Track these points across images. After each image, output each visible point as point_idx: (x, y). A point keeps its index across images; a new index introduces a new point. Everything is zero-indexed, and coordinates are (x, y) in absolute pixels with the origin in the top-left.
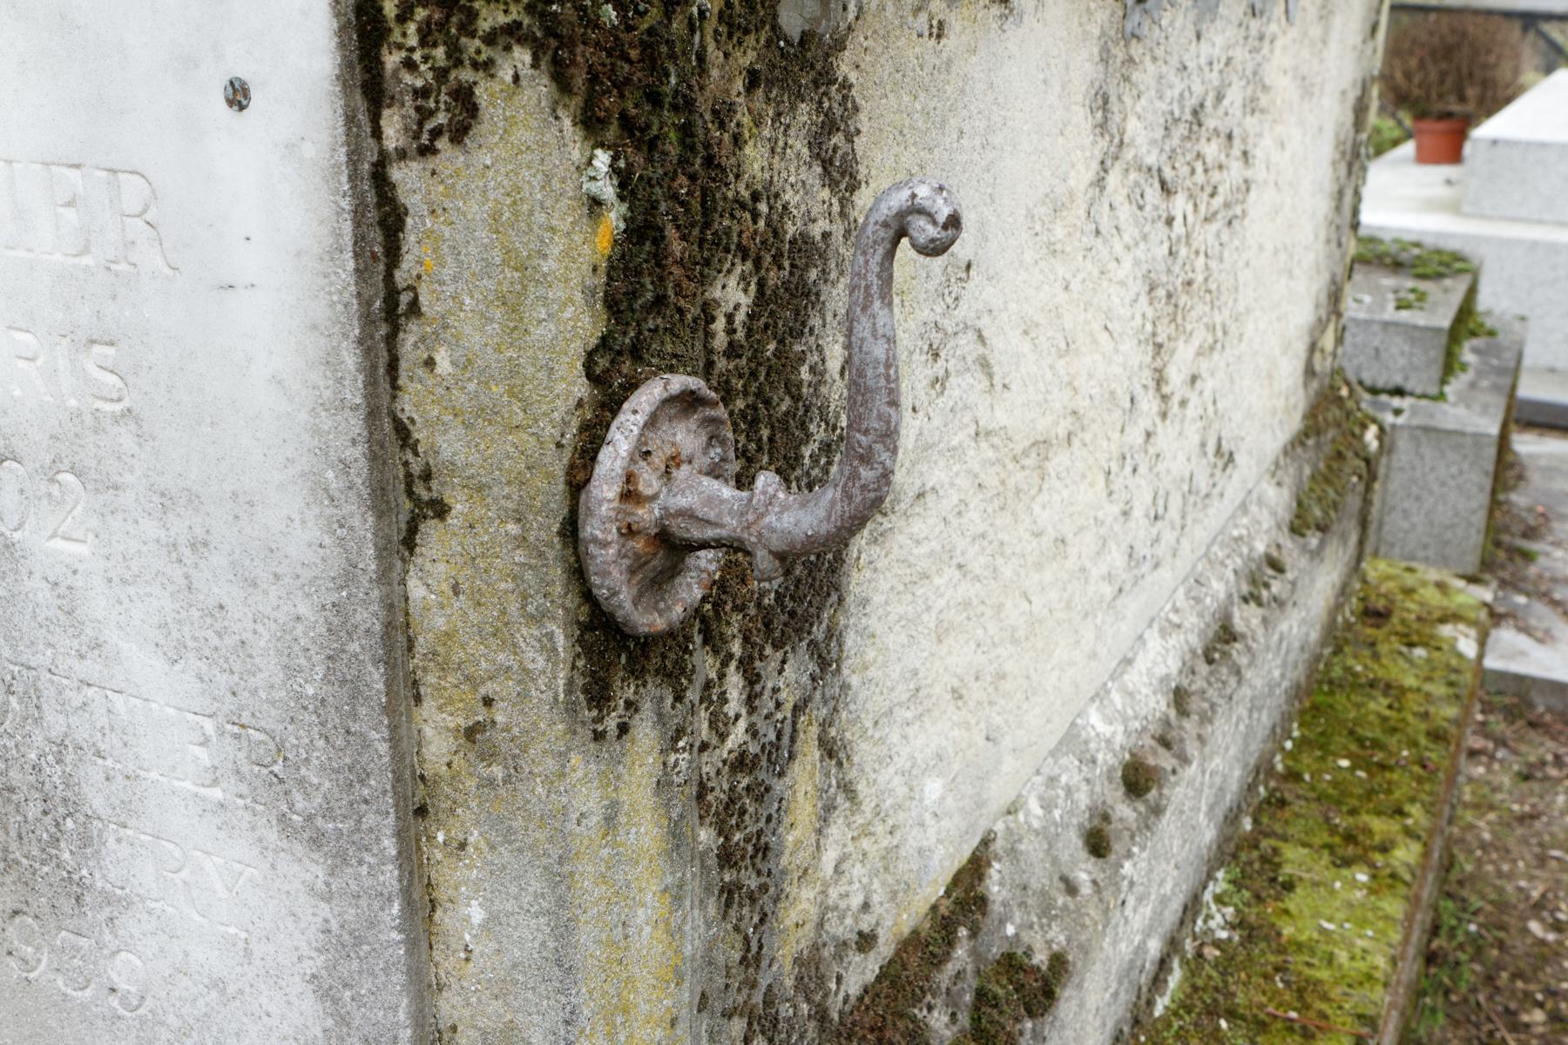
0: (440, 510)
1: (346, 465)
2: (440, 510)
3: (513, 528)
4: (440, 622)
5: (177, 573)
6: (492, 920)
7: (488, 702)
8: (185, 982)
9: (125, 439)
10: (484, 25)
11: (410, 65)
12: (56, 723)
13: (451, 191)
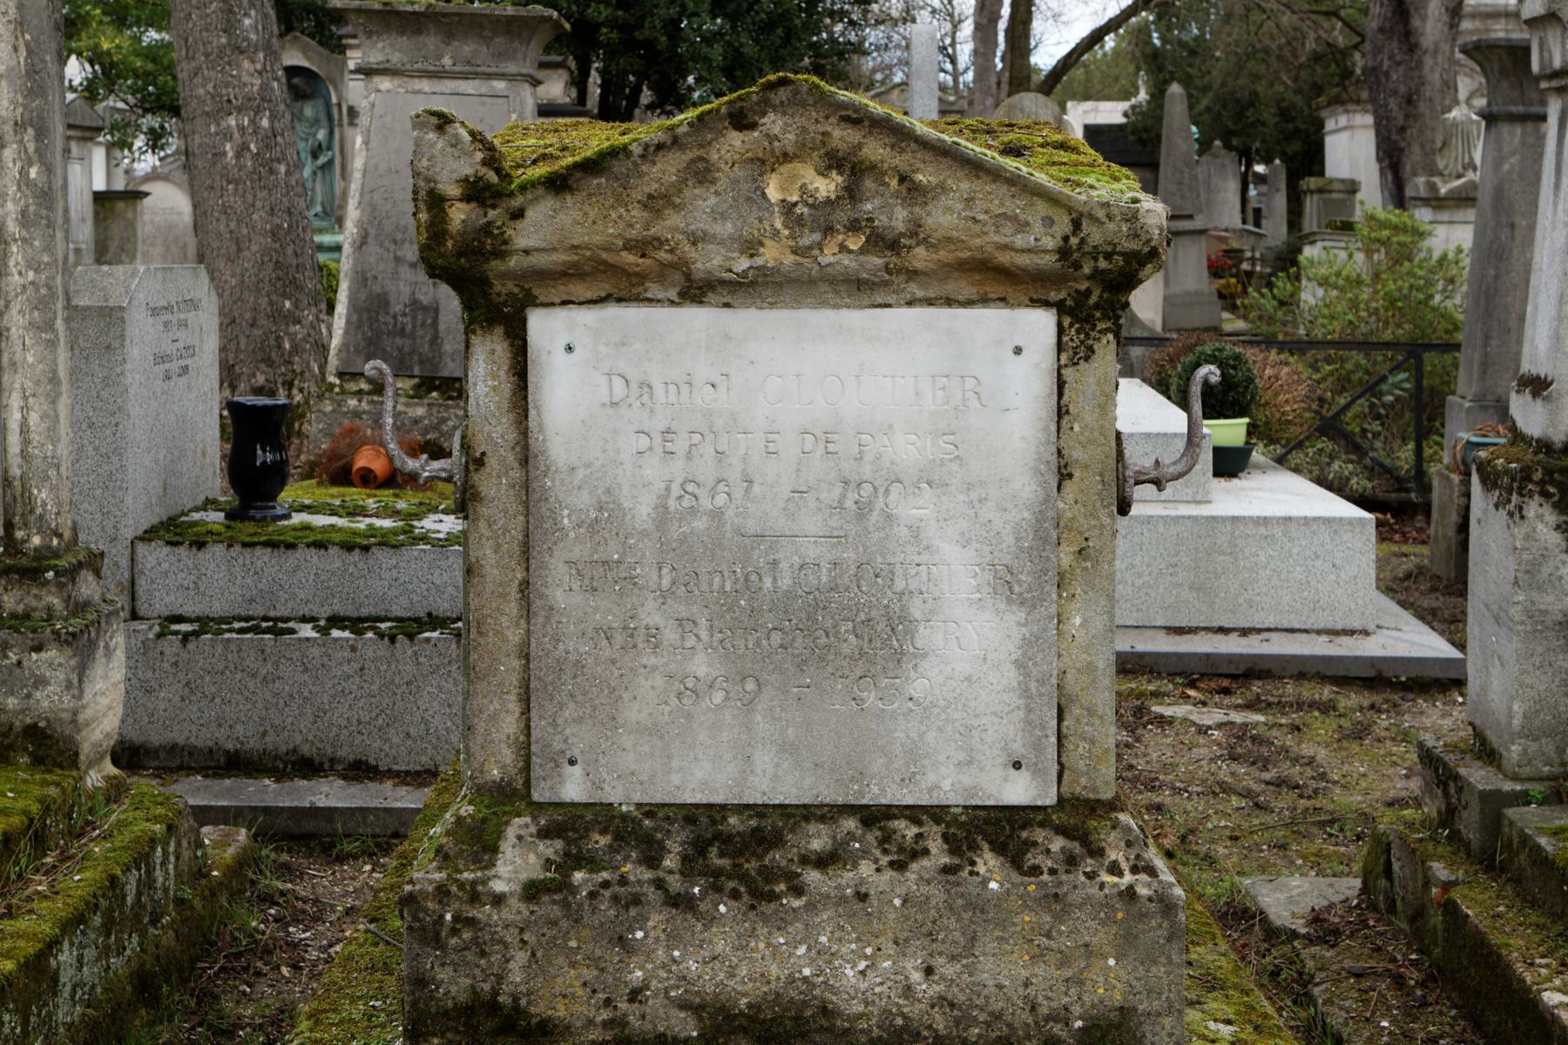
0: (1070, 476)
1: (1048, 462)
2: (1070, 476)
3: (1098, 478)
4: (1069, 515)
5: (972, 513)
6: (1085, 621)
7: (1086, 539)
8: (951, 682)
9: (955, 467)
10: (1098, 328)
11: (1072, 340)
12: (900, 584)
13: (1083, 376)
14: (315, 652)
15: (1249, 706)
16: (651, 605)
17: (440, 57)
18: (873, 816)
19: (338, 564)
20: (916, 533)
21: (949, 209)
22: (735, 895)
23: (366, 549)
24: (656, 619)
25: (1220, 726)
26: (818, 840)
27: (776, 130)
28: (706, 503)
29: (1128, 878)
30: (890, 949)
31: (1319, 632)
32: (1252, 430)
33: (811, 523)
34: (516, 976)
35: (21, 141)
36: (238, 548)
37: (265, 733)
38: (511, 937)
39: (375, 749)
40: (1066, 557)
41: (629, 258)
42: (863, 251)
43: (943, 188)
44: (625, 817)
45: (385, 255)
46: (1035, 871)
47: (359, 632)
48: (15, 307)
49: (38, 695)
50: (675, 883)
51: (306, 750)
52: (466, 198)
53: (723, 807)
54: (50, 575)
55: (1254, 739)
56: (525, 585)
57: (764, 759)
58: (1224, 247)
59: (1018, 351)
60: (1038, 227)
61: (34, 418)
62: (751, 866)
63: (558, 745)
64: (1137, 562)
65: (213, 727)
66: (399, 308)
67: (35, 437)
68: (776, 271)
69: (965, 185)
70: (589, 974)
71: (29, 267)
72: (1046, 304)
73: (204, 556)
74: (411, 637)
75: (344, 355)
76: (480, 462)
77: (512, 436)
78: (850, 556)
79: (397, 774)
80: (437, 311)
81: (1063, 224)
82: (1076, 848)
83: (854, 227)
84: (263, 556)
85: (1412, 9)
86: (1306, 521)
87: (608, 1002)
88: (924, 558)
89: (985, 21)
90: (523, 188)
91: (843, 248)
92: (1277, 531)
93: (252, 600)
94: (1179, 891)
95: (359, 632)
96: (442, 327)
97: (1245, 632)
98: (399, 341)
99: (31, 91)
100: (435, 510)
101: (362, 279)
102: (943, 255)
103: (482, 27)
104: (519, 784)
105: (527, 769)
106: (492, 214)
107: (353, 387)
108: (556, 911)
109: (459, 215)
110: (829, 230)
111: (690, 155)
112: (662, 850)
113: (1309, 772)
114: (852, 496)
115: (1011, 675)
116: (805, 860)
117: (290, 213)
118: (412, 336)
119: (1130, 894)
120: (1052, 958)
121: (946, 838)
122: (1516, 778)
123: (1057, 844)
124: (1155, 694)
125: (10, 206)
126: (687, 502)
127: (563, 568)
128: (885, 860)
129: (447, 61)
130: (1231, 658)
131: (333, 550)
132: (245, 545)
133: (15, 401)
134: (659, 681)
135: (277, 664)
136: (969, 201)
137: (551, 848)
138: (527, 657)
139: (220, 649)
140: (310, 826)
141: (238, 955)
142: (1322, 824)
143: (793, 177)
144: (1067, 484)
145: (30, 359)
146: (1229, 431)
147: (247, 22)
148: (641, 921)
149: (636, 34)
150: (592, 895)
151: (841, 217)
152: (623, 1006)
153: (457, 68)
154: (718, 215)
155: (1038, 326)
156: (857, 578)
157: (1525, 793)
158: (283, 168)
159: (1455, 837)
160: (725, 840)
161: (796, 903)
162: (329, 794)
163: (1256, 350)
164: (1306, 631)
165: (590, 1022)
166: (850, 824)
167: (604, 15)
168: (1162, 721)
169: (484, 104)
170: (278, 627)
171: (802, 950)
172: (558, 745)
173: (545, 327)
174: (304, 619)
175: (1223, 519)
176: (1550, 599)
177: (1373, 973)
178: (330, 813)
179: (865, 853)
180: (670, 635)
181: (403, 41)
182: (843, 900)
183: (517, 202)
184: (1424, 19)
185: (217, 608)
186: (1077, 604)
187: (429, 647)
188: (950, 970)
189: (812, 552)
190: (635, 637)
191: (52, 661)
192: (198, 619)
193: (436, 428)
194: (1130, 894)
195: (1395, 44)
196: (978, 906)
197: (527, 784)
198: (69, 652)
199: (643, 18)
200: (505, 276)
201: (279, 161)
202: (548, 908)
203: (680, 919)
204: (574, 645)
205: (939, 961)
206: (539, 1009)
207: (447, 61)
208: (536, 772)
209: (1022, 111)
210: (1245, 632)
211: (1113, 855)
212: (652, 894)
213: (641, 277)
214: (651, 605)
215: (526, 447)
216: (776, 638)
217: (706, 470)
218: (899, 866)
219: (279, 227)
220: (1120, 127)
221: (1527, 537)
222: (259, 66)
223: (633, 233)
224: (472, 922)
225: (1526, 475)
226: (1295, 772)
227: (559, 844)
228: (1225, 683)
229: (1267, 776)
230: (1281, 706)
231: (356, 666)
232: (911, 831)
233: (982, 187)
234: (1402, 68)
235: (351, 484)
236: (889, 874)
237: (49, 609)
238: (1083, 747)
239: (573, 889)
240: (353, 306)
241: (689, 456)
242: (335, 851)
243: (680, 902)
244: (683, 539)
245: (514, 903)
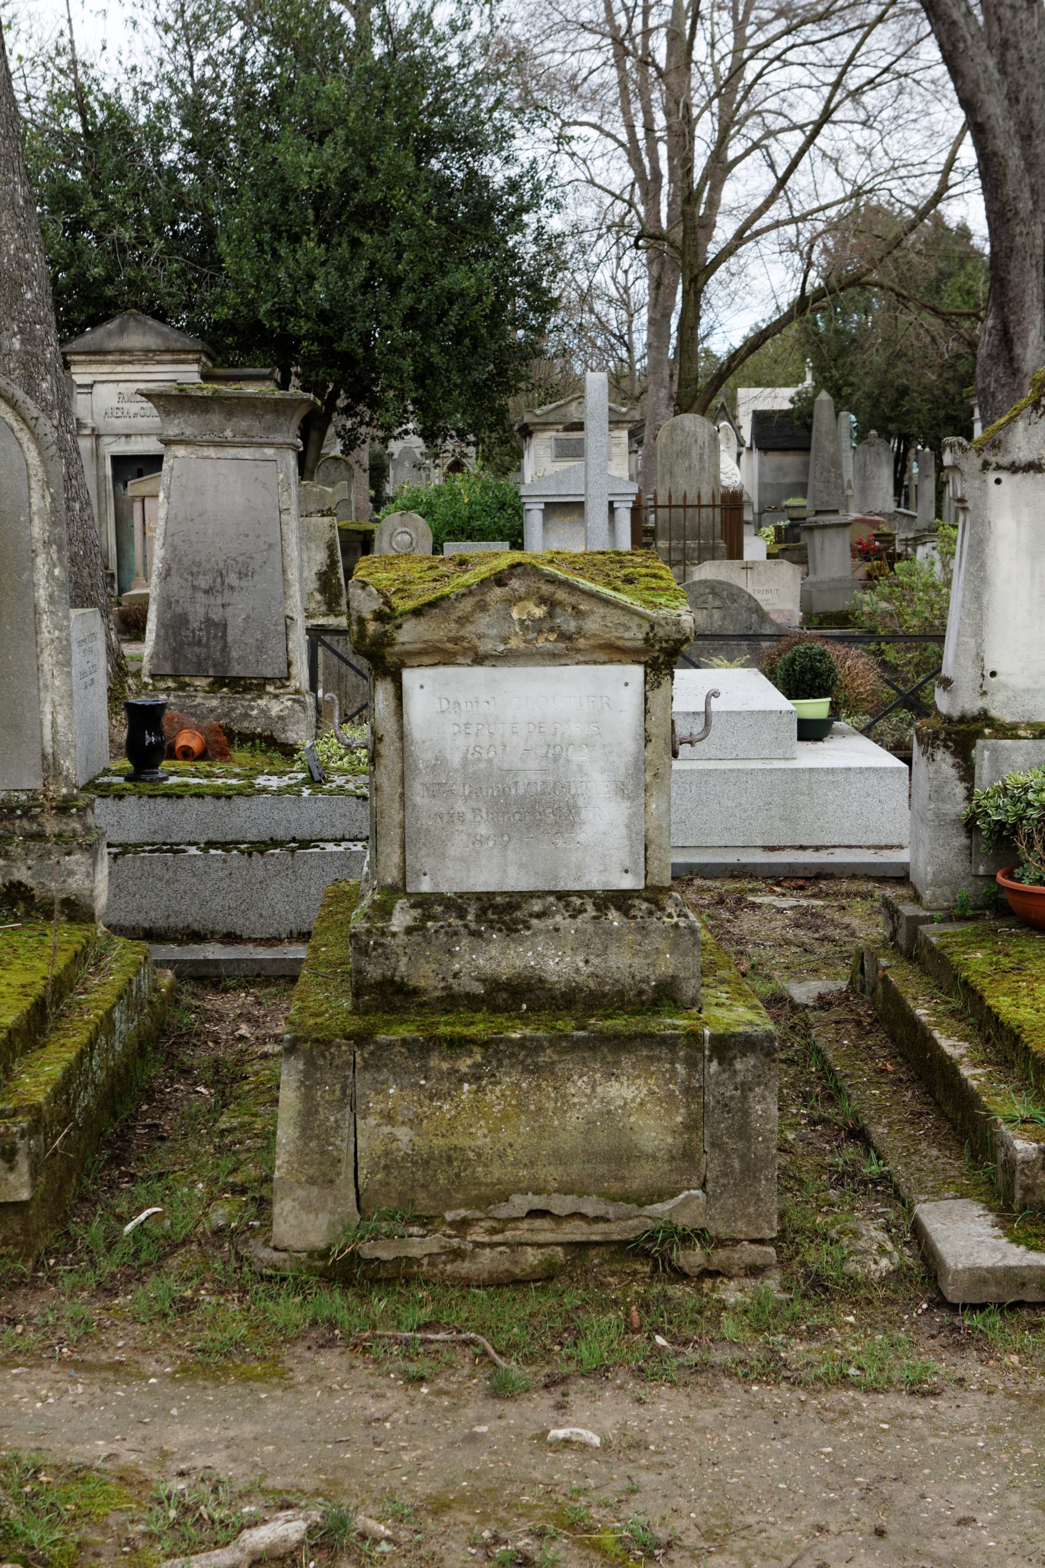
12: (573, 791)
14: (200, 863)
15: (814, 896)
16: (460, 803)
17: (223, 430)
18: (562, 896)
19: (211, 807)
20: (580, 768)
21: (594, 622)
22: (500, 930)
23: (229, 797)
24: (463, 809)
25: (792, 908)
26: (537, 906)
27: (516, 586)
28: (485, 756)
29: (676, 919)
30: (569, 952)
31: (869, 847)
32: (834, 708)
33: (533, 764)
34: (402, 968)
35: (48, 553)
36: (145, 798)
37: (169, 916)
38: (400, 951)
39: (240, 925)
40: (648, 777)
41: (449, 645)
42: (556, 641)
43: (592, 612)
44: (449, 898)
45: (184, 584)
46: (634, 917)
47: (228, 851)
48: (46, 652)
49: (70, 880)
50: (473, 926)
51: (195, 926)
52: (375, 619)
53: (494, 893)
54: (74, 810)
55: (812, 915)
56: (402, 795)
57: (512, 871)
58: (876, 532)
59: (626, 684)
60: (635, 628)
61: (60, 719)
62: (507, 918)
63: (418, 867)
64: (743, 802)
65: (135, 913)
66: (196, 625)
67: (61, 730)
68: (517, 650)
69: (602, 610)
70: (435, 966)
71: (56, 628)
72: (639, 663)
73: (124, 804)
74: (262, 853)
75: (155, 661)
76: (381, 739)
77: (395, 727)
78: (550, 779)
79: (255, 940)
80: (225, 626)
81: (646, 627)
82: (653, 907)
83: (552, 630)
84: (162, 802)
85: (1015, 339)
86: (861, 770)
87: (443, 979)
88: (585, 779)
89: (658, 317)
90: (401, 615)
91: (547, 640)
92: (841, 778)
93: (155, 832)
94: (698, 924)
95: (228, 851)
96: (229, 639)
97: (817, 848)
98: (197, 650)
99: (54, 523)
100: (262, 773)
101: (167, 603)
102: (592, 642)
103: (255, 407)
104: (400, 885)
105: (404, 878)
106: (387, 627)
107: (162, 685)
108: (420, 939)
109: (372, 627)
110: (540, 632)
111: (477, 598)
112: (467, 912)
113: (845, 932)
114: (551, 751)
115: (624, 831)
116: (531, 915)
117: (85, 543)
118: (207, 646)
119: (676, 926)
120: (642, 955)
121: (594, 904)
122: (928, 909)
123: (645, 906)
124: (752, 890)
125: (42, 592)
126: (476, 755)
127: (420, 787)
128: (567, 914)
129: (228, 433)
130: (806, 866)
131: (208, 799)
132: (150, 796)
133: (47, 708)
134: (464, 837)
135: (175, 872)
136: (604, 617)
137: (417, 913)
138: (404, 828)
139: (138, 863)
140: (204, 971)
141: (182, 1036)
142: (844, 958)
143: (524, 608)
144: (649, 745)
145: (57, 683)
146: (817, 708)
147: (44, 385)
148: (458, 942)
149: (335, 345)
150: (436, 932)
151: (546, 625)
152: (450, 980)
153: (236, 439)
154: (490, 626)
155: (636, 673)
156: (554, 789)
157: (932, 917)
158: (77, 506)
159: (896, 945)
160: (495, 907)
161: (528, 933)
162: (213, 952)
163: (839, 647)
164: (860, 847)
165: (436, 988)
166: (551, 899)
167: (305, 328)
168: (754, 906)
169: (257, 466)
170: (174, 849)
171: (530, 954)
172: (418, 867)
173: (410, 677)
174: (190, 844)
175: (804, 770)
176: (949, 806)
177: (846, 1021)
178: (217, 962)
179: (558, 912)
180: (469, 816)
181: (194, 418)
182: (549, 931)
183: (399, 621)
184: (1025, 347)
185: (133, 838)
186: (653, 799)
187: (274, 859)
188: (595, 961)
189: (533, 777)
190: (453, 817)
191: (77, 860)
192: (120, 845)
193: (226, 715)
194: (676, 926)
195: (1001, 369)
196: (608, 932)
197: (404, 885)
198: (87, 855)
199: (341, 331)
200: (392, 654)
201: (74, 500)
202: (416, 937)
203: (476, 941)
204: (425, 822)
205: (591, 957)
206: (413, 983)
207: (228, 433)
208: (408, 879)
209: (683, 430)
210: (817, 848)
211: (669, 910)
212: (463, 931)
213: (455, 654)
214: (460, 803)
215: (402, 732)
216: (517, 816)
217: (485, 741)
218: (573, 917)
219: (76, 554)
220: (785, 414)
221: (936, 772)
222: (55, 422)
223: (452, 634)
224: (382, 945)
225: (936, 736)
226: (836, 934)
227: (420, 911)
228: (801, 882)
229: (816, 936)
230: (836, 895)
231: (227, 872)
232: (579, 902)
233: (609, 611)
234: (1007, 389)
235: (176, 758)
236: (569, 920)
237: (74, 830)
238: (656, 863)
239: (428, 930)
240: (161, 624)
241: (477, 735)
242: (221, 986)
243: (475, 934)
244: (475, 773)
245: (401, 936)
